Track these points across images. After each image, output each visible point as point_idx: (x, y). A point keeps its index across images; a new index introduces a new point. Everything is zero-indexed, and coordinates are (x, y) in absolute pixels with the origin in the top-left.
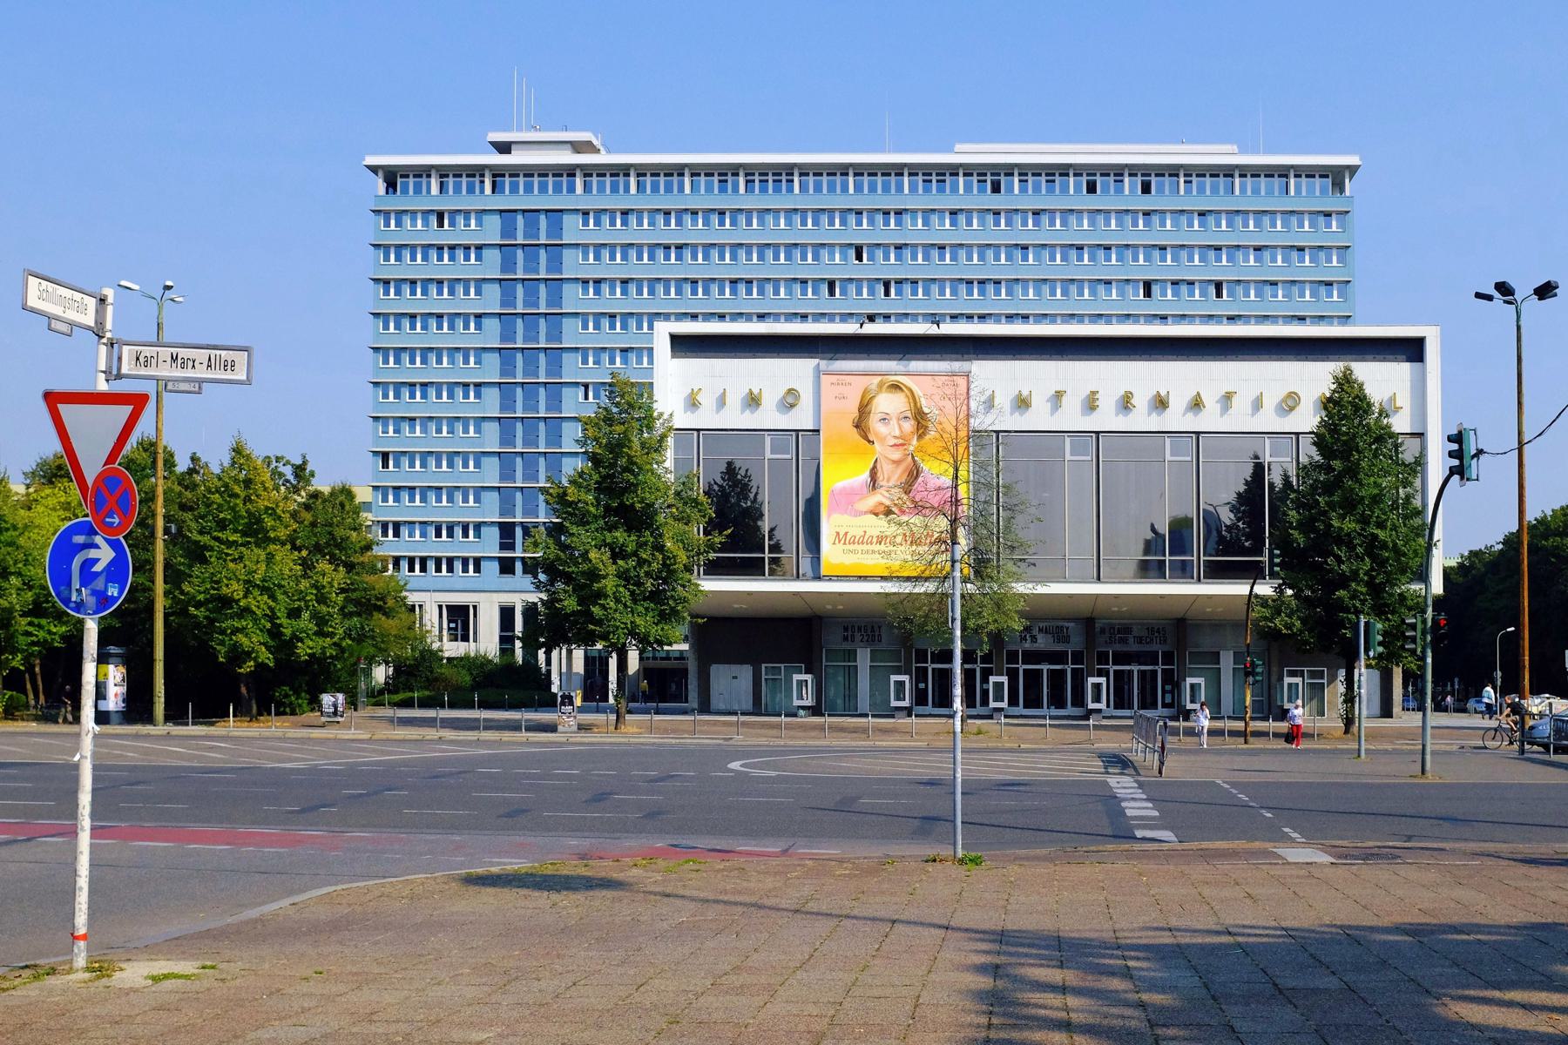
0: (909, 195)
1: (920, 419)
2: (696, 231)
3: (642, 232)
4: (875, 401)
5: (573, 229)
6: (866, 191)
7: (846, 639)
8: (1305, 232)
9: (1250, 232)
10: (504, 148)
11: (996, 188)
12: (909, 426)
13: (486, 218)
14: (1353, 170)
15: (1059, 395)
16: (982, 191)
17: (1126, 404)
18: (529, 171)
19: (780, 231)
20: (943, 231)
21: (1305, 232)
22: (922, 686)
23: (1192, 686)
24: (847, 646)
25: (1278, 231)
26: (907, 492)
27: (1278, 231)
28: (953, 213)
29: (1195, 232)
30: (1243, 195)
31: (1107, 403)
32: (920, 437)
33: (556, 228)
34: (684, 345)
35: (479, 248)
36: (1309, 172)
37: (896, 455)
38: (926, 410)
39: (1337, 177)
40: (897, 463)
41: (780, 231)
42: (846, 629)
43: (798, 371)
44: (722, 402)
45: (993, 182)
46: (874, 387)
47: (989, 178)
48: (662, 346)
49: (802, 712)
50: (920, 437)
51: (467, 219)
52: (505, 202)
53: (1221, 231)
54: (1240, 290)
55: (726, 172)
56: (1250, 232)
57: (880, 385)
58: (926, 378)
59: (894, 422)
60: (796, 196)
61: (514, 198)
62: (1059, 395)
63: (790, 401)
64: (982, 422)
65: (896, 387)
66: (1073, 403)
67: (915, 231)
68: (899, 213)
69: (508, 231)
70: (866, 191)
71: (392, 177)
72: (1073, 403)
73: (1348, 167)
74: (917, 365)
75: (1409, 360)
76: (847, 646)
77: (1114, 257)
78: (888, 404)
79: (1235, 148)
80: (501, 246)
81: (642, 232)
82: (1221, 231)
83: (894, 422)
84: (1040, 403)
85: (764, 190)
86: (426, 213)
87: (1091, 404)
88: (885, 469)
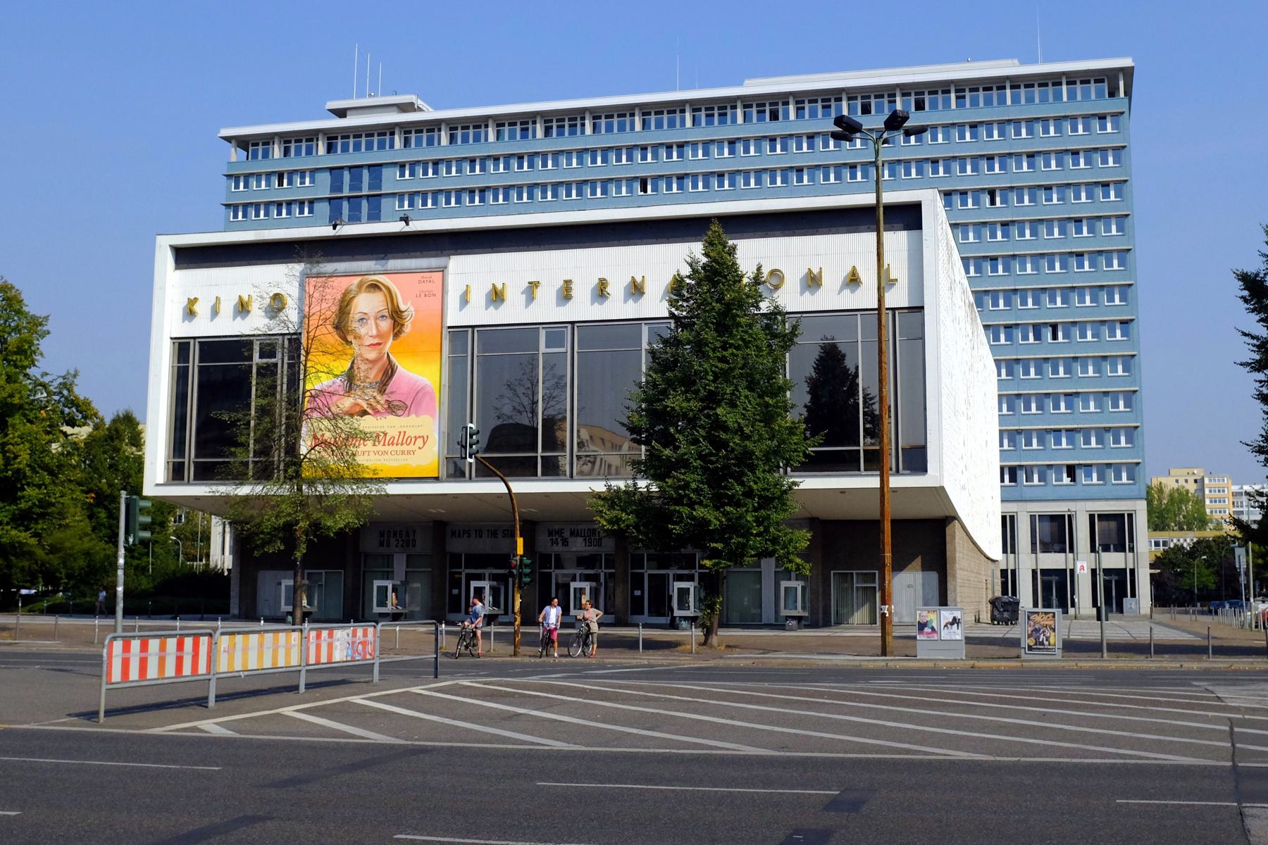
0: (688, 129)
1: (396, 316)
2: (497, 175)
3: (451, 178)
4: (355, 300)
5: (392, 181)
6: (665, 126)
7: (382, 544)
8: (1079, 136)
9: (1023, 140)
10: (341, 113)
11: (774, 116)
12: (386, 325)
13: (318, 176)
14: (1128, 73)
15: (533, 285)
16: (761, 119)
17: (601, 291)
18: (357, 132)
19: (572, 169)
20: (722, 159)
21: (1079, 136)
22: (637, 593)
23: (379, 588)
24: (383, 550)
25: (1050, 137)
26: (382, 391)
27: (1050, 137)
28: (732, 142)
29: (967, 144)
30: (1010, 106)
31: (582, 292)
32: (396, 335)
33: (376, 182)
34: (187, 257)
35: (311, 202)
36: (1085, 78)
37: (372, 355)
38: (403, 307)
39: (1112, 81)
40: (374, 362)
41: (572, 169)
42: (382, 534)
43: (281, 277)
44: (215, 312)
45: (771, 112)
46: (354, 287)
47: (767, 109)
48: (165, 259)
49: (684, 624)
50: (396, 335)
51: (303, 178)
52: (338, 160)
53: (993, 142)
54: (1013, 197)
55: (524, 122)
56: (1023, 140)
57: (360, 285)
58: (404, 279)
59: (372, 322)
60: (588, 136)
61: (357, 154)
62: (533, 285)
63: (276, 305)
64: (455, 318)
65: (375, 287)
66: (547, 294)
67: (696, 161)
68: (681, 146)
69: (336, 186)
70: (665, 126)
71: (243, 143)
72: (547, 294)
73: (1122, 70)
74: (394, 264)
75: (907, 227)
76: (383, 550)
77: (1112, 193)
78: (367, 304)
79: (1016, 61)
80: (330, 199)
81: (451, 178)
82: (993, 142)
83: (372, 322)
84: (514, 296)
85: (560, 134)
86: (269, 175)
87: (566, 293)
88: (362, 369)
